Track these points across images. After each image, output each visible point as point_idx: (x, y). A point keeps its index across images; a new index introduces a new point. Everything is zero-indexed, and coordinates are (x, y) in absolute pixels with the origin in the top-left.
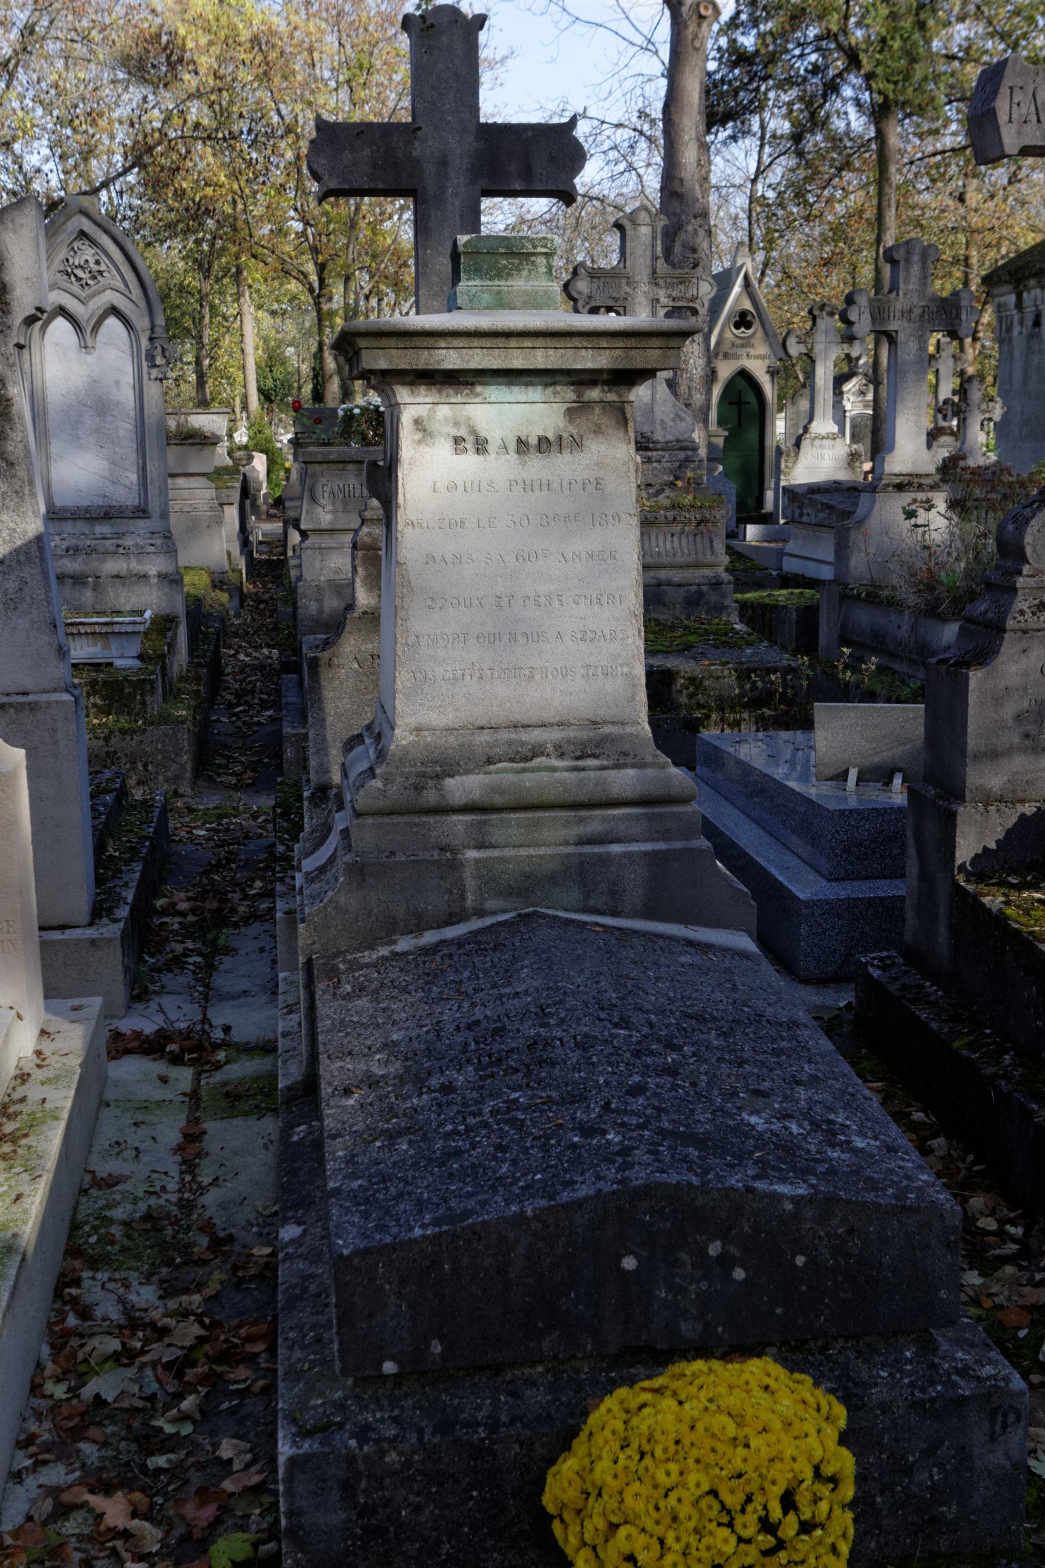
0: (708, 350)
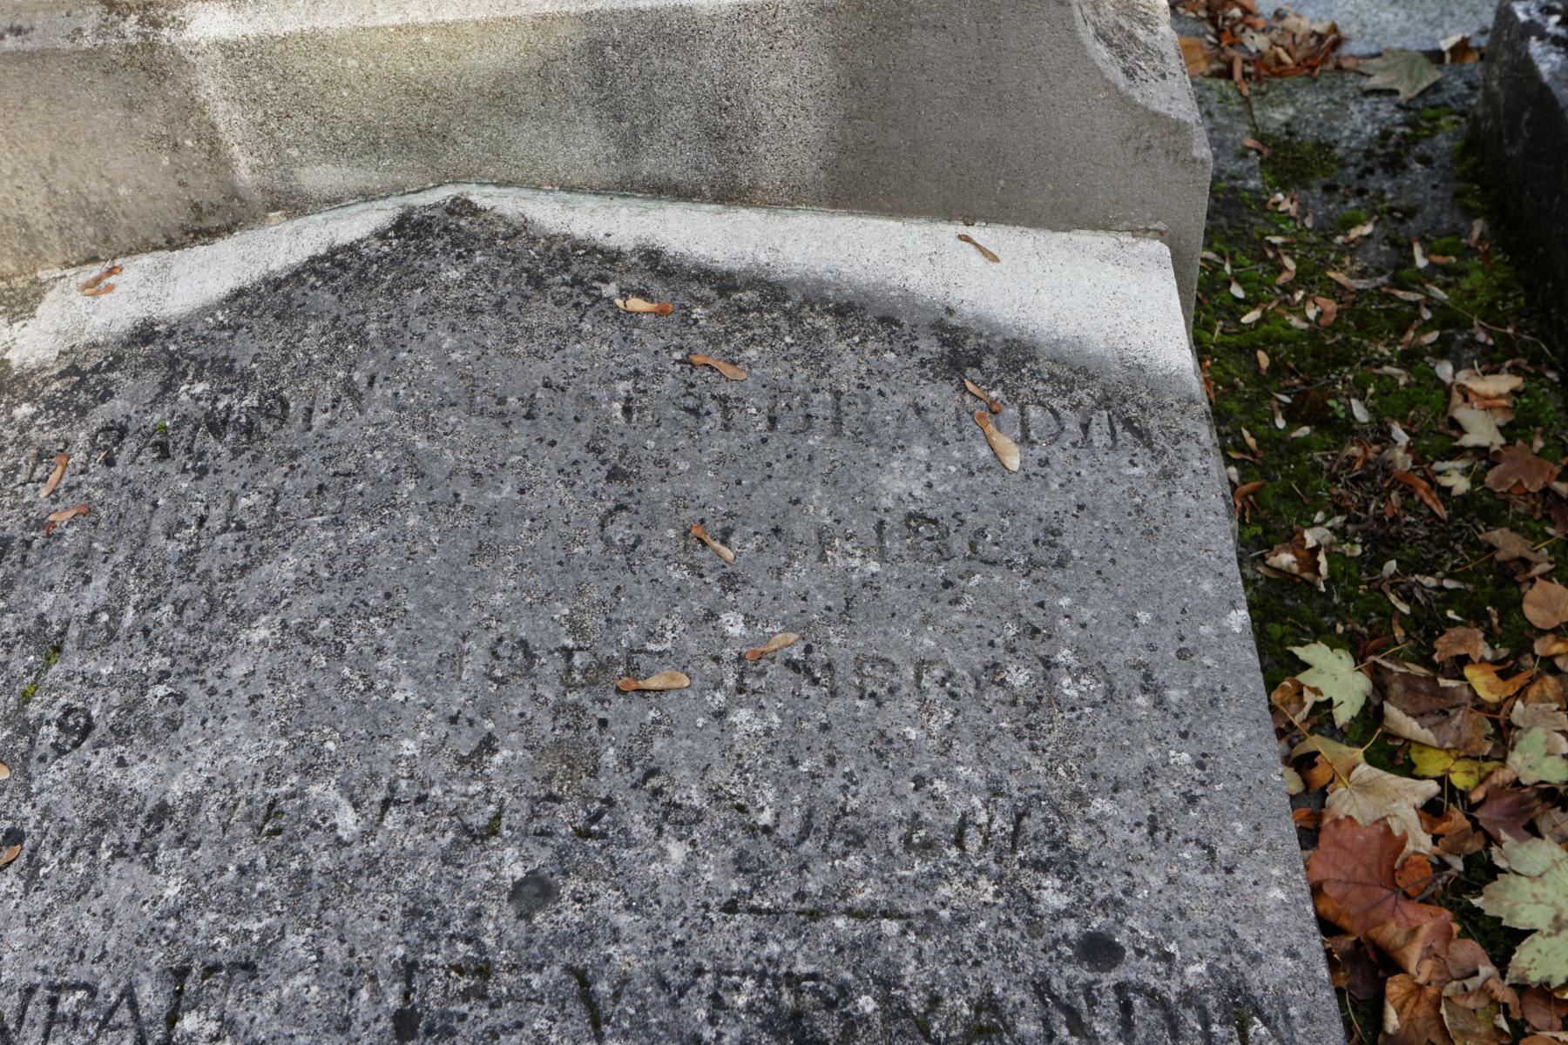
0: (1461, 623)
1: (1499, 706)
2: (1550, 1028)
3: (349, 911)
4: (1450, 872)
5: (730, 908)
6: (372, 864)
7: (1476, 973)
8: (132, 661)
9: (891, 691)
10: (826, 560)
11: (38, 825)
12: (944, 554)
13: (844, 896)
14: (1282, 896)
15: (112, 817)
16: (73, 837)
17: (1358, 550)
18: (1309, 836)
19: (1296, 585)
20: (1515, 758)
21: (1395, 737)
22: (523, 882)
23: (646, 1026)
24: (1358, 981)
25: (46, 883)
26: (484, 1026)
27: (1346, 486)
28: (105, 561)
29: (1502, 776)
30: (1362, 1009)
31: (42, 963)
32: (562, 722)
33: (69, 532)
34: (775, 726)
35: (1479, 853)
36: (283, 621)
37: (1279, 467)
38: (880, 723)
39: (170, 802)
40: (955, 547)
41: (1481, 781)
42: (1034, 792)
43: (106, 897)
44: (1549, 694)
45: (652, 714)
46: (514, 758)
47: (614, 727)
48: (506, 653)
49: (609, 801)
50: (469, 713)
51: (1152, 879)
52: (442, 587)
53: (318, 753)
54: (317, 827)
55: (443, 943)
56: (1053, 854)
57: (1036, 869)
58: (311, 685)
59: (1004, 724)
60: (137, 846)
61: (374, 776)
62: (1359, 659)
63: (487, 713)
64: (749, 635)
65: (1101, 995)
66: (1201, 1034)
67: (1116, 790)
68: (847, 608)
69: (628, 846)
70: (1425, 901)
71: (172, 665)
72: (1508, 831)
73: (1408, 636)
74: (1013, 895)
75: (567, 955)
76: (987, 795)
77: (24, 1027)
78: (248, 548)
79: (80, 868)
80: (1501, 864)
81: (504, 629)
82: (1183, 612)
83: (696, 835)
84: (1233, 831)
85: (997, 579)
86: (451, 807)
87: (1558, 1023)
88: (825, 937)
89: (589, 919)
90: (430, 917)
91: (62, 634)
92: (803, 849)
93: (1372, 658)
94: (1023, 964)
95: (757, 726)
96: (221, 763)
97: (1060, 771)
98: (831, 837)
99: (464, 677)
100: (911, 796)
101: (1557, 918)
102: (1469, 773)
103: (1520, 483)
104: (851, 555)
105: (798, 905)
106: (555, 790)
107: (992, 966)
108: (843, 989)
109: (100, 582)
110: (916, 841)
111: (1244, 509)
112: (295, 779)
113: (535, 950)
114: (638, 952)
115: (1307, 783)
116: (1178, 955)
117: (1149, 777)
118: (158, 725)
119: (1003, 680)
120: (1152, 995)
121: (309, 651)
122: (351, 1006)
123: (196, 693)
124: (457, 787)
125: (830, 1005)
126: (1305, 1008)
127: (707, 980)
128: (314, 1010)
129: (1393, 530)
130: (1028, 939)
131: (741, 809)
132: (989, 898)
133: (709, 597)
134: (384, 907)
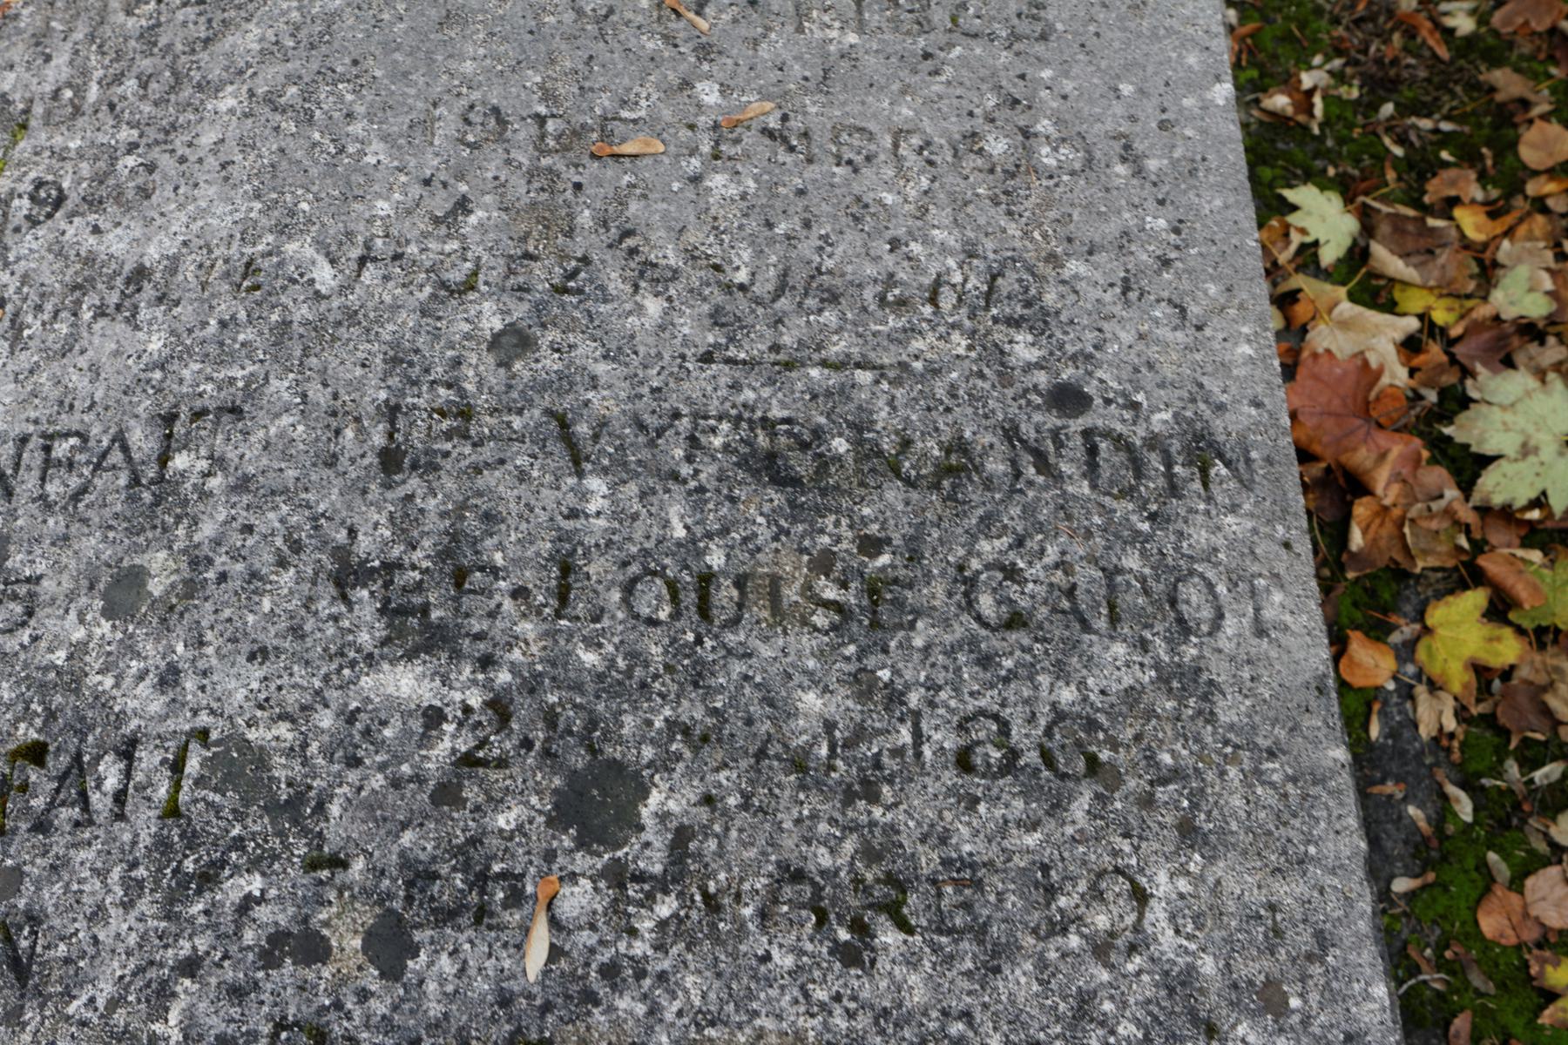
1: (1485, 246)
2: (1509, 546)
3: (330, 358)
4: (1424, 403)
5: (707, 358)
6: (351, 316)
7: (1441, 496)
8: (100, 135)
9: (868, 159)
10: (803, 32)
11: (19, 291)
12: (924, 26)
13: (819, 348)
14: (1251, 352)
15: (91, 281)
16: (54, 300)
17: (1355, 93)
18: (1289, 372)
19: (1289, 128)
20: (1498, 296)
21: (1379, 276)
22: (502, 333)
23: (625, 464)
24: (1326, 503)
25: (31, 343)
26: (467, 462)
27: (1347, 28)
28: (64, 40)
29: (1483, 311)
30: (1327, 530)
31: (33, 415)
32: (536, 185)
33: (25, 12)
34: (751, 191)
35: (1453, 386)
36: (250, 90)
37: (1280, 10)
38: (857, 188)
39: (148, 265)
40: (936, 19)
41: (1462, 317)
42: (1009, 254)
43: (90, 353)
44: (1537, 233)
45: (627, 178)
46: (489, 218)
47: (589, 190)
48: (478, 119)
49: (585, 260)
50: (443, 176)
51: (1123, 335)
52: (411, 54)
53: (292, 213)
54: (295, 281)
55: (425, 388)
56: (1026, 311)
57: (1009, 325)
58: (282, 150)
59: (980, 191)
60: (118, 307)
61: (349, 234)
62: (1348, 200)
63: (460, 176)
64: (724, 103)
65: (1068, 439)
66: (1163, 475)
67: (1090, 253)
68: (825, 78)
69: (605, 301)
70: (1397, 430)
71: (141, 136)
72: (1485, 364)
73: (1400, 179)
74: (985, 349)
75: (547, 400)
76: (962, 257)
77: (21, 472)
78: (210, 21)
79: (63, 328)
80: (1474, 394)
81: (476, 95)
82: (1167, 84)
83: (672, 292)
84: (1206, 293)
85: (978, 51)
86: (428, 264)
87: (1517, 541)
88: (799, 386)
89: (568, 367)
90: (411, 364)
91: (26, 111)
92: (778, 305)
93: (1361, 199)
94: (993, 411)
95: (733, 191)
96: (195, 227)
97: (1036, 235)
98: (806, 294)
99: (436, 142)
100: (886, 257)
101: (1524, 445)
102: (1450, 309)
103: (1526, 23)
104: (829, 27)
105: (773, 357)
106: (531, 249)
107: (962, 412)
108: (818, 433)
109: (61, 59)
110: (890, 298)
111: (1240, 51)
112: (270, 238)
113: (515, 395)
114: (616, 398)
115: (1288, 320)
116: (1145, 404)
117: (1124, 241)
118: (130, 194)
119: (982, 149)
120: (1119, 441)
121: (278, 117)
122: (337, 444)
123: (166, 162)
124: (433, 245)
125: (804, 446)
126: (1266, 452)
127: (684, 424)
128: (302, 447)
129: (1392, 72)
130: (999, 388)
131: (717, 268)
132: (961, 351)
133: (683, 67)
134: (365, 355)
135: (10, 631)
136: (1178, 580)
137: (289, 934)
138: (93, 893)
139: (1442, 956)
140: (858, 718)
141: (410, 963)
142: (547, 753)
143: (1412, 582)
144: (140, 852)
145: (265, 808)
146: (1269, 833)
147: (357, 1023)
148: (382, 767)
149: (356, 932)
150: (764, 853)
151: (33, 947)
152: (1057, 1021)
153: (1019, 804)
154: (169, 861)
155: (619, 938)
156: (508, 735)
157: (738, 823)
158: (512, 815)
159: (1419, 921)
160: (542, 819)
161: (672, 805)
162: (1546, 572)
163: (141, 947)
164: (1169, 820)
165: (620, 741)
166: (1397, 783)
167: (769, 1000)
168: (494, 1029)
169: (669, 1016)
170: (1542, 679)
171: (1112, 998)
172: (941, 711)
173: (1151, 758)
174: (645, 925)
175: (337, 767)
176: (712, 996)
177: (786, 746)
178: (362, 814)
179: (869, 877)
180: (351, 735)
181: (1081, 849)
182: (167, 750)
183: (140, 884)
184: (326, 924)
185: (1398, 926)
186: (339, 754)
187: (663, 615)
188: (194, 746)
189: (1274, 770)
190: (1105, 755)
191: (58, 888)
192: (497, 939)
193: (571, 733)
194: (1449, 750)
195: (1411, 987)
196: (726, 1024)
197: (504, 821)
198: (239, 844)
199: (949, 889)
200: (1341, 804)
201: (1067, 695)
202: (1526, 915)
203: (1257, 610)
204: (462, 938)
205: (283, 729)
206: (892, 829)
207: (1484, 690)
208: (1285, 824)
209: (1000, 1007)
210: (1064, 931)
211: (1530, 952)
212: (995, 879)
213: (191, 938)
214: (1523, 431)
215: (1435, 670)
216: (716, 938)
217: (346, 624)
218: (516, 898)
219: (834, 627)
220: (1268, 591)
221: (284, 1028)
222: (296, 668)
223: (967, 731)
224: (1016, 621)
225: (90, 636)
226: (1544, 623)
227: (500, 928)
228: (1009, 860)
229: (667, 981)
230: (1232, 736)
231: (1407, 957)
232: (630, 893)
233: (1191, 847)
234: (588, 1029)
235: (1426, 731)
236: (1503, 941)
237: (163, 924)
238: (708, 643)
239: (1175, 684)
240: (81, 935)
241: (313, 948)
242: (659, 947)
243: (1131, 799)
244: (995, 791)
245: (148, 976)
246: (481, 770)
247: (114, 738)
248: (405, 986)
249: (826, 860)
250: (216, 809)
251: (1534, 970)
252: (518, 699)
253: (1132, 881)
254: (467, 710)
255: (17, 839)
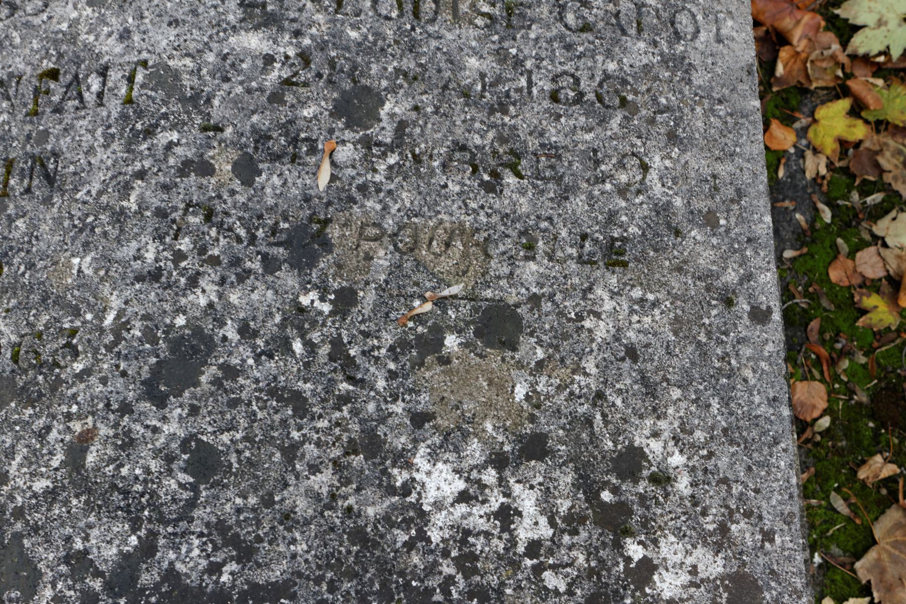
2: (866, 76)
7: (830, 48)
24: (764, 50)
30: (764, 66)
87: (871, 74)
135: (36, 15)
136: (676, 12)
137: (193, 161)
138: (87, 141)
139: (808, 290)
140: (498, 72)
141: (257, 179)
142: (330, 81)
143: (809, 96)
144: (112, 120)
145: (179, 99)
146: (716, 140)
147: (229, 205)
148: (241, 83)
149: (228, 162)
150: (445, 136)
151: (56, 168)
152: (597, 224)
153: (583, 119)
154: (128, 125)
155: (368, 172)
156: (309, 71)
157: (432, 120)
158: (311, 110)
159: (797, 273)
160: (327, 113)
161: (397, 110)
162: (885, 92)
163: (114, 166)
164: (662, 131)
165: (370, 77)
166: (791, 201)
167: (446, 206)
168: (301, 212)
169: (393, 211)
170: (877, 148)
171: (626, 215)
172: (543, 71)
173: (655, 100)
174: (382, 167)
175: (217, 81)
176: (416, 203)
177: (459, 85)
178: (231, 105)
179: (501, 151)
180: (224, 66)
181: (615, 143)
182: (125, 71)
183: (113, 136)
184: (213, 158)
185: (785, 275)
186: (218, 75)
187: (394, 15)
188: (139, 68)
189: (721, 110)
190: (630, 97)
191: (68, 139)
192: (303, 170)
193: (343, 72)
194: (821, 185)
195: (789, 306)
196: (423, 216)
197: (307, 112)
198: (165, 116)
199: (544, 159)
200: (756, 128)
201: (612, 66)
202: (855, 271)
203: (718, 30)
204: (284, 168)
205: (188, 61)
206: (514, 128)
207: (843, 154)
208: (725, 136)
209: (567, 216)
210: (603, 182)
211: (855, 289)
212: (568, 154)
213: (141, 161)
214: (879, 12)
215: (817, 142)
216: (419, 176)
217: (221, 10)
218: (313, 150)
219: (487, 26)
220: (725, 19)
221: (191, 206)
222: (194, 31)
223: (557, 82)
224: (586, 28)
225: (80, 16)
226: (881, 118)
227: (304, 164)
228: (576, 146)
229: (393, 194)
230: (699, 91)
231: (789, 290)
232: (374, 151)
233: (674, 145)
234: (351, 215)
235: (809, 175)
236: (841, 284)
237: (126, 155)
238: (418, 30)
239: (671, 64)
240: (82, 161)
241: (206, 169)
242: (389, 178)
243: (643, 120)
244: (570, 112)
245: (119, 179)
246: (294, 88)
247: (96, 66)
248: (254, 189)
249: (478, 141)
250: (153, 99)
251: (856, 299)
252: (314, 53)
253: (641, 160)
254: (287, 57)
255: (45, 117)
